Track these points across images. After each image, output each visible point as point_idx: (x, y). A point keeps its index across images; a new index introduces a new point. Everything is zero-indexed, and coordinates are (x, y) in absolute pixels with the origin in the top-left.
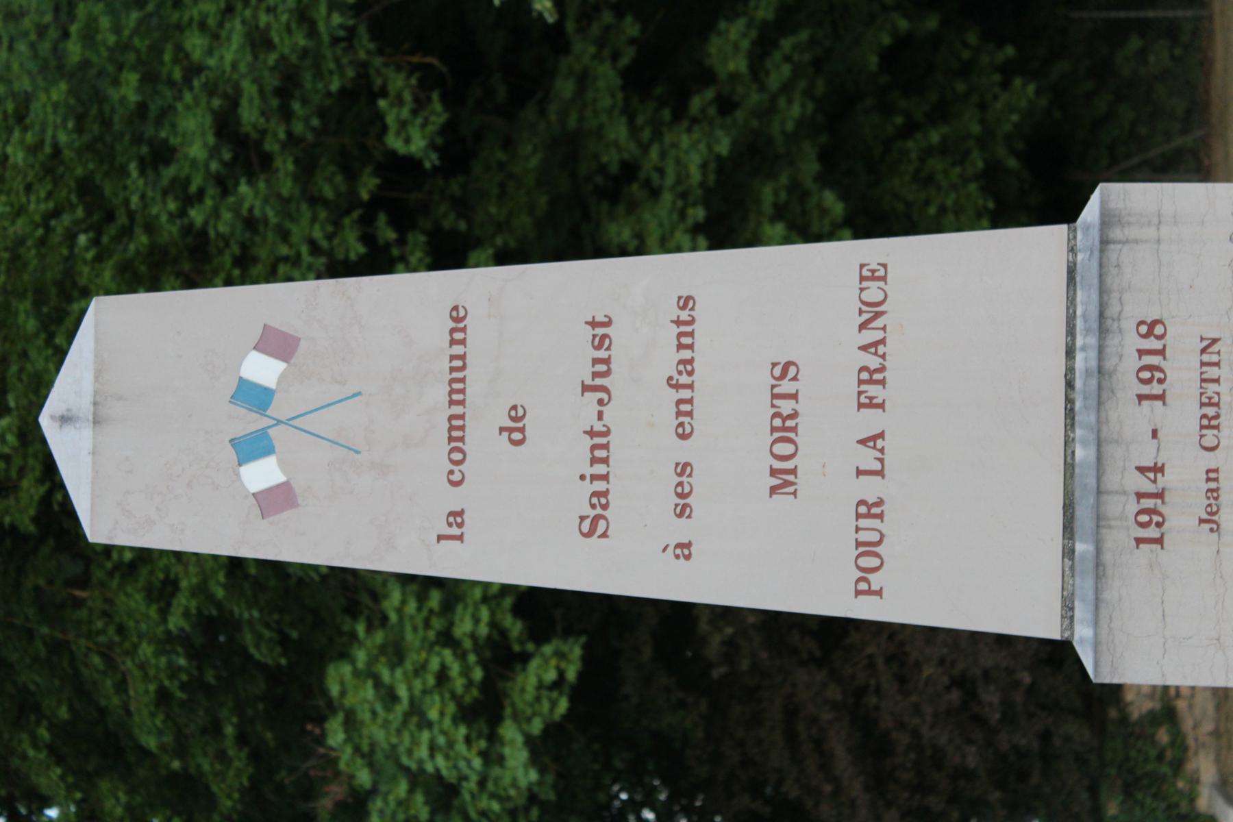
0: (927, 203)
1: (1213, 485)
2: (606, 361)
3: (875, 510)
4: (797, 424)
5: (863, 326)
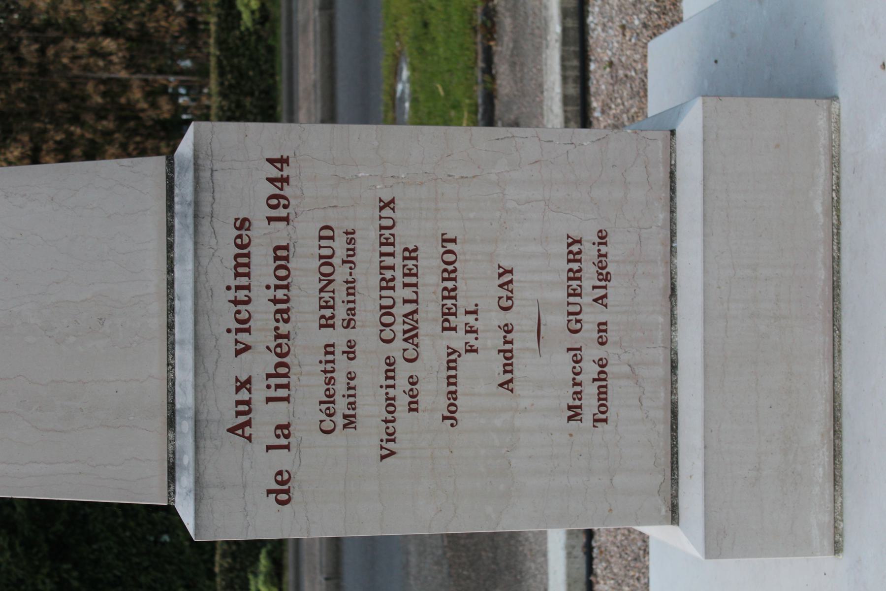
2: (353, 250)
4: (417, 255)
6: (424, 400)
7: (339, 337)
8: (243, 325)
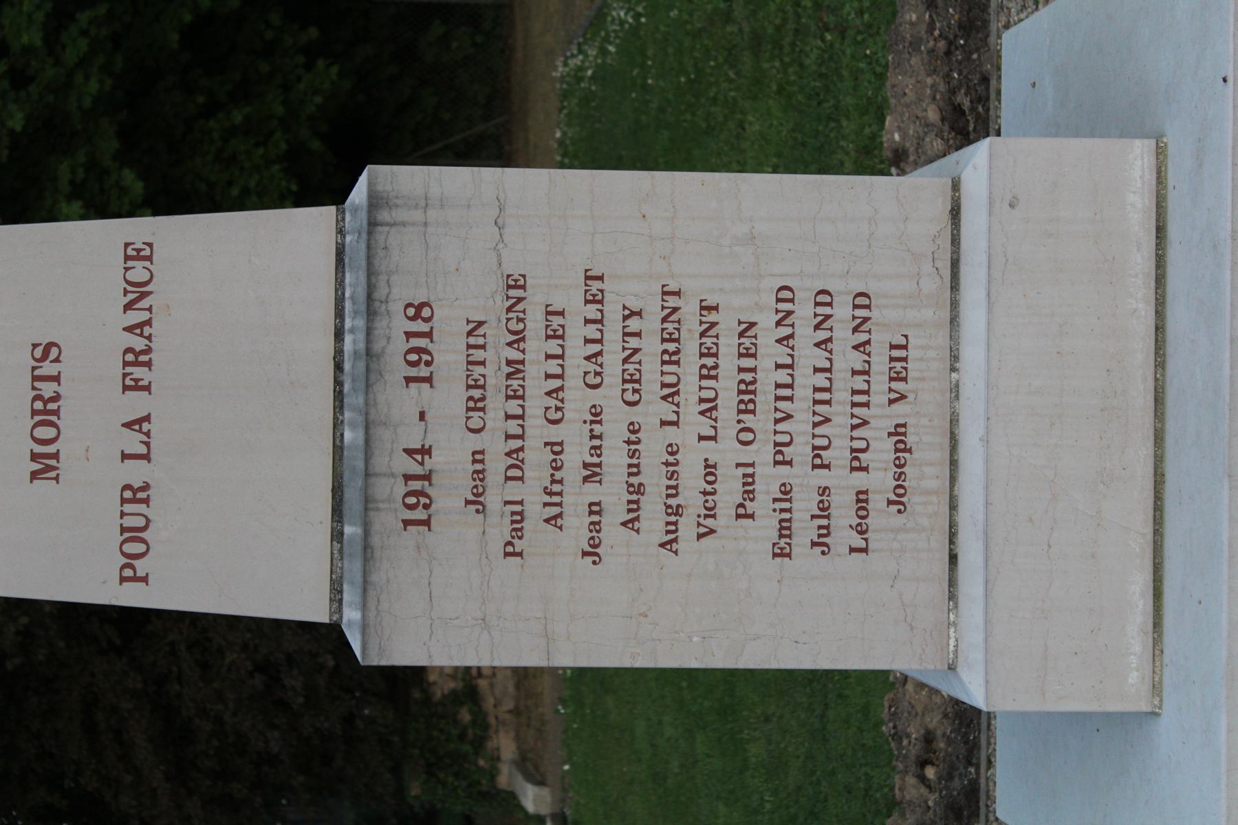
0: (230, 184)
1: (479, 467)
3: (140, 495)
5: (128, 307)
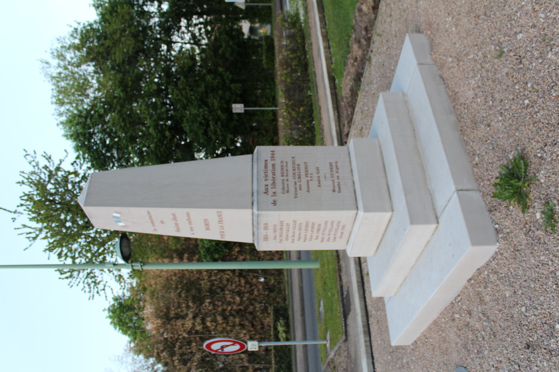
6: (302, 188)
7: (285, 178)
8: (266, 176)
